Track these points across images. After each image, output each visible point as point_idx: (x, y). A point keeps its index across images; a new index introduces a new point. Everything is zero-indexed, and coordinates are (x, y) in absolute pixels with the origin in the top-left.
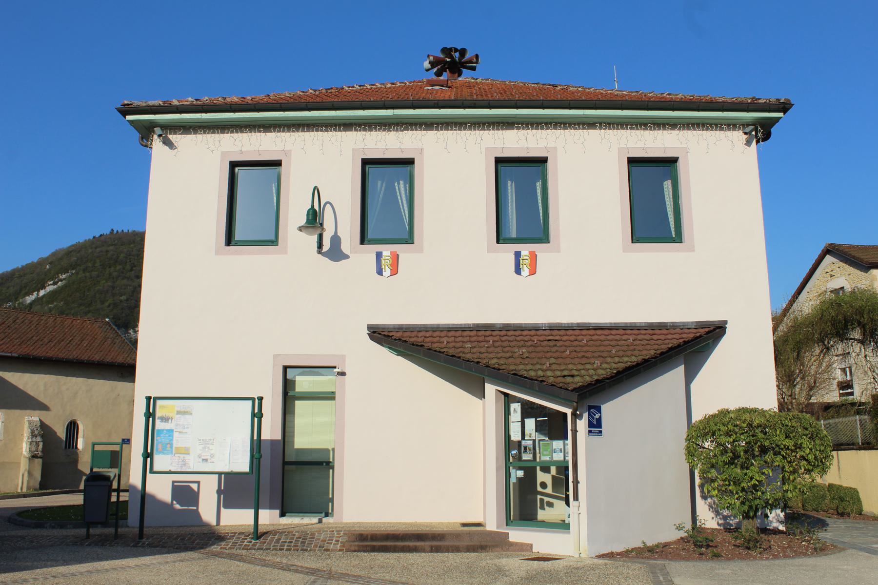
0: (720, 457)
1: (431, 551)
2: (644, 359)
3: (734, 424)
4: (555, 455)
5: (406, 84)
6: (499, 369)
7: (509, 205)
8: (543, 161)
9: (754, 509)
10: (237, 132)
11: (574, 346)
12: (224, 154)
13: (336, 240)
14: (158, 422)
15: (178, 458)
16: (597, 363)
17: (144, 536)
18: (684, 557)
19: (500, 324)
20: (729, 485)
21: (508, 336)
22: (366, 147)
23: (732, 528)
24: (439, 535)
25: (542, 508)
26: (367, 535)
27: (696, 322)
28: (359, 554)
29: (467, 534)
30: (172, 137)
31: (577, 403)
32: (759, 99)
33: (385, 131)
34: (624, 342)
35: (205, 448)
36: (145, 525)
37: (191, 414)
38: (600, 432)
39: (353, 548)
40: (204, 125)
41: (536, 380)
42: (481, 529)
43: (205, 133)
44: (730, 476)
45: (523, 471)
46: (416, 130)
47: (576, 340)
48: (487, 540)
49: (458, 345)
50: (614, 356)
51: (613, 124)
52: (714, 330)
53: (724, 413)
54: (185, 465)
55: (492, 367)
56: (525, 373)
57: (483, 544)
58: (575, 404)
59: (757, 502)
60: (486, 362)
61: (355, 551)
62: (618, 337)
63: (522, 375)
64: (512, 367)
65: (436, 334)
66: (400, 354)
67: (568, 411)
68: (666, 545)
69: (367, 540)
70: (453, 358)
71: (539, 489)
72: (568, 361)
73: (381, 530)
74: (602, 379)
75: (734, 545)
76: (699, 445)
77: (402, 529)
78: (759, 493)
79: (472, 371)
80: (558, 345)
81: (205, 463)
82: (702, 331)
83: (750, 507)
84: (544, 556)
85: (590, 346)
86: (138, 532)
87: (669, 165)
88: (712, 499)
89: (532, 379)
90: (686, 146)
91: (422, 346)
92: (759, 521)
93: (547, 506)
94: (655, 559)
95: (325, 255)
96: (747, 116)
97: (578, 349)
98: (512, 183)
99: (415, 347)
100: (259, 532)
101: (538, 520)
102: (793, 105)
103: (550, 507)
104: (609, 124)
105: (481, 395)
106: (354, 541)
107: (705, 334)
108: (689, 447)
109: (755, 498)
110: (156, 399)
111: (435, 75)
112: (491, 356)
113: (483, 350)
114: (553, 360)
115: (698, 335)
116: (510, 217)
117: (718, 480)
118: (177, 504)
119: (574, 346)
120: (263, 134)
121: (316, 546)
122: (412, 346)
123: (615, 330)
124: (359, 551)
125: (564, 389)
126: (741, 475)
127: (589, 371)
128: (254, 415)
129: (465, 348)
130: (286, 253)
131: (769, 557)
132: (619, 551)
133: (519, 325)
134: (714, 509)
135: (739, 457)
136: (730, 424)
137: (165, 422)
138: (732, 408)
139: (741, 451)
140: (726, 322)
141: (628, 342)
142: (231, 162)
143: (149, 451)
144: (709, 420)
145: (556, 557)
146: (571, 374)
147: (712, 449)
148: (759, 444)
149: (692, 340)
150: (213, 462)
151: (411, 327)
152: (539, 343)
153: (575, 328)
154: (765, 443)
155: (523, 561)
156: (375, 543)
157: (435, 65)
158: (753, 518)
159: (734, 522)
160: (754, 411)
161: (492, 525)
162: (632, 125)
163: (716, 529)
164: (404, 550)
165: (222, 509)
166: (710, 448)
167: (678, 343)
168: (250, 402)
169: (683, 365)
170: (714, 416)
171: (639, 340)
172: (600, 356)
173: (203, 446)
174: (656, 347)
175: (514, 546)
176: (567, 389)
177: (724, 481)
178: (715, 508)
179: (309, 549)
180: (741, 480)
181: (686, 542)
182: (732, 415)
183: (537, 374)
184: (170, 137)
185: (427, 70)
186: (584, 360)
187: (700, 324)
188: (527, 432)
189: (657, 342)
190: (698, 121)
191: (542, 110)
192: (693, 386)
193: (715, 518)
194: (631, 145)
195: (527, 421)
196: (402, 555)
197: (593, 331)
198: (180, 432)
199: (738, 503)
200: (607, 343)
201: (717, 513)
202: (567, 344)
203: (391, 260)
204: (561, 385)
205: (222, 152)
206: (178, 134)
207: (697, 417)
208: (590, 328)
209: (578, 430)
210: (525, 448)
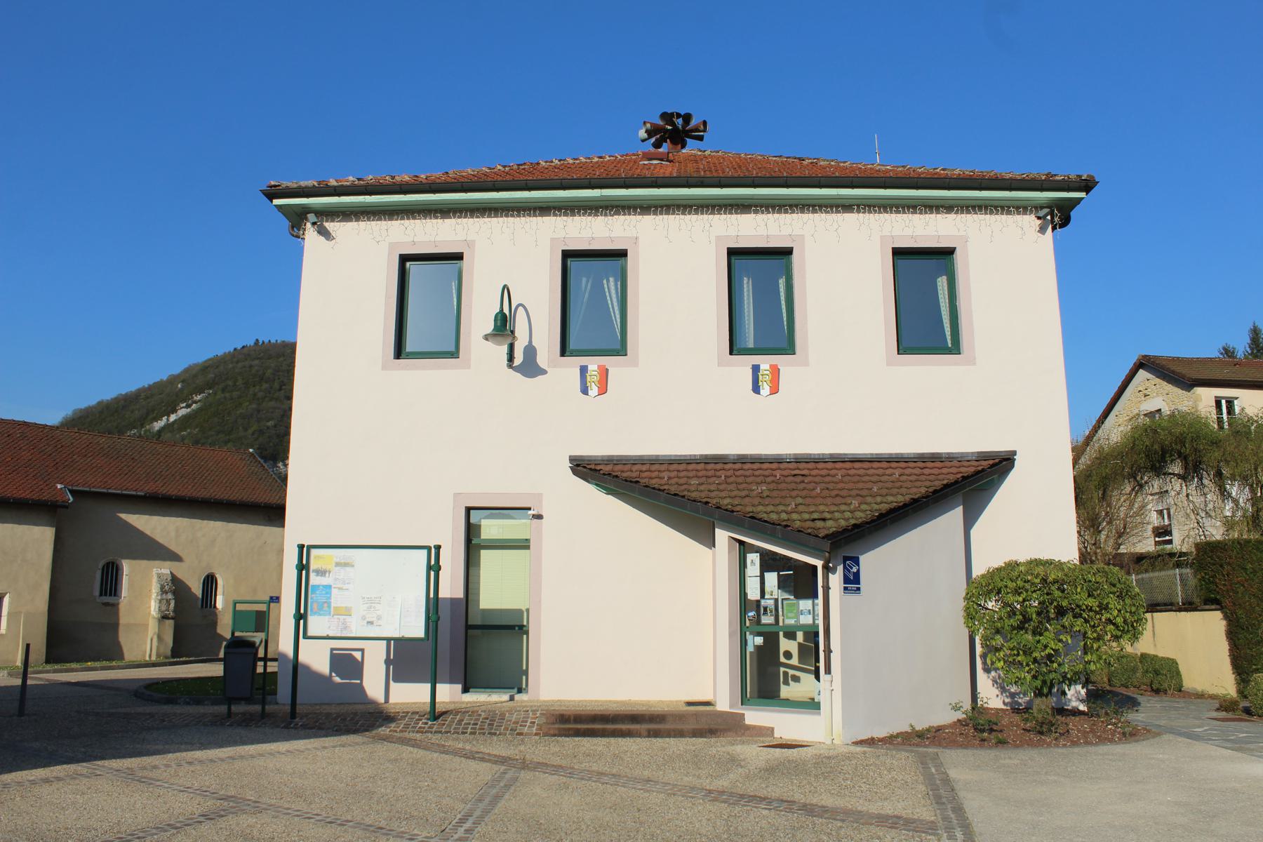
0: (1006, 620)
1: (649, 736)
6: (733, 511)
10: (408, 219)
11: (826, 483)
13: (530, 351)
14: (312, 575)
16: (855, 503)
17: (297, 715)
18: (961, 743)
19: (734, 455)
20: (1018, 655)
24: (658, 715)
25: (786, 683)
26: (569, 716)
29: (693, 715)
32: (1055, 175)
34: (888, 477)
36: (298, 702)
37: (353, 566)
38: (858, 589)
39: (552, 732)
41: (779, 525)
44: (1019, 644)
49: (682, 481)
51: (874, 207)
52: (1001, 462)
53: (1012, 565)
56: (765, 516)
58: (827, 554)
59: (1052, 676)
61: (555, 735)
64: (749, 509)
66: (610, 492)
67: (819, 563)
68: (939, 729)
71: (782, 659)
75: (1024, 729)
76: (980, 605)
77: (614, 709)
78: (1055, 665)
79: (698, 513)
81: (370, 626)
82: (985, 464)
83: (1044, 682)
84: (789, 743)
88: (996, 672)
89: (773, 524)
90: (964, 233)
92: (1054, 699)
93: (792, 680)
94: (926, 746)
95: (517, 369)
97: (831, 486)
98: (749, 280)
100: (437, 711)
104: (869, 206)
105: (711, 543)
107: (989, 468)
108: (968, 608)
109: (1050, 672)
110: (310, 547)
112: (723, 494)
113: (712, 487)
114: (799, 500)
115: (980, 468)
117: (1004, 648)
118: (337, 676)
119: (826, 483)
120: (440, 221)
121: (506, 729)
127: (845, 513)
128: (429, 568)
129: (690, 484)
130: (469, 368)
135: (1031, 620)
137: (321, 576)
140: (1014, 453)
141: (893, 478)
144: (993, 574)
145: (803, 744)
146: (823, 517)
147: (997, 610)
148: (1055, 604)
149: (972, 476)
150: (380, 626)
152: (782, 478)
153: (827, 460)
156: (579, 726)
158: (1047, 696)
160: (1049, 563)
163: (1002, 709)
165: (391, 682)
168: (425, 552)
170: (999, 570)
172: (858, 495)
174: (928, 483)
176: (817, 536)
177: (1012, 649)
178: (1001, 684)
179: (498, 732)
180: (1032, 649)
181: (964, 726)
182: (1022, 568)
184: (327, 225)
185: (643, 141)
186: (838, 500)
188: (767, 589)
190: (974, 203)
192: (973, 532)
193: (1000, 696)
195: (767, 575)
196: (612, 740)
197: (849, 463)
198: (339, 588)
199: (1029, 677)
200: (867, 478)
201: (1003, 689)
202: (817, 479)
204: (809, 531)
205: (390, 243)
207: (978, 570)
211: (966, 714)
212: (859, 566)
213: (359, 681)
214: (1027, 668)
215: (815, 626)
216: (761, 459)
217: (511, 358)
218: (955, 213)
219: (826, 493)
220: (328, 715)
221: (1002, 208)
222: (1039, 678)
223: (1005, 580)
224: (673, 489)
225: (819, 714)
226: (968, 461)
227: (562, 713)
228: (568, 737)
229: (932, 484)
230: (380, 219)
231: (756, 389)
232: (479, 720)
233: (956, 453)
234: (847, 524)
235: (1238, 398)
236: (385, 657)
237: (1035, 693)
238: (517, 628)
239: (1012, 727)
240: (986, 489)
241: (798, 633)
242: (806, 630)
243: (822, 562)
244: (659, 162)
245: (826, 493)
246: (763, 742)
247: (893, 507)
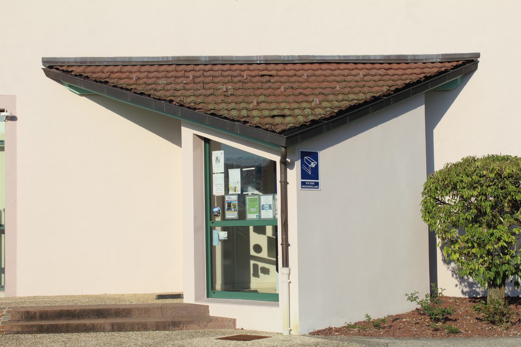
0: (461, 214)
1: (113, 330)
2: (374, 97)
3: (479, 174)
4: (263, 212)
6: (195, 109)
9: (502, 276)
11: (291, 82)
16: (317, 100)
18: (415, 333)
19: (205, 57)
20: (473, 247)
21: (214, 71)
23: (478, 296)
24: (124, 310)
25: (256, 275)
26: (35, 313)
27: (443, 55)
28: (22, 336)
29: (158, 308)
31: (285, 148)
34: (352, 77)
38: (317, 184)
39: (15, 329)
41: (238, 121)
42: (178, 302)
44: (473, 237)
45: (227, 232)
47: (295, 75)
48: (182, 315)
49: (150, 81)
50: (338, 93)
52: (464, 64)
53: (469, 161)
56: (225, 113)
57: (176, 320)
58: (283, 149)
59: (505, 267)
60: (180, 101)
61: (18, 333)
62: (346, 72)
63: (222, 115)
64: (211, 106)
65: (125, 69)
66: (83, 93)
67: (277, 159)
68: (397, 318)
69: (36, 318)
70: (143, 96)
71: (253, 253)
72: (281, 99)
74: (320, 119)
75: (477, 319)
76: (438, 200)
77: (84, 304)
78: (508, 257)
79: (163, 111)
82: (448, 65)
83: (497, 273)
84: (248, 334)
85: (311, 82)
89: (233, 120)
91: (106, 82)
92: (510, 288)
93: (262, 272)
94: (379, 337)
97: (295, 85)
99: (98, 84)
101: (251, 289)
105: (177, 140)
106: (19, 320)
107: (452, 69)
108: (426, 202)
109: (503, 263)
112: (189, 93)
113: (179, 87)
114: (262, 98)
115: (443, 69)
117: (459, 240)
119: (291, 82)
122: (94, 83)
123: (344, 64)
125: (271, 131)
126: (487, 235)
127: (305, 110)
129: (158, 84)
131: (516, 334)
132: (339, 327)
133: (228, 59)
134: (458, 275)
135: (485, 214)
136: (475, 174)
138: (480, 155)
139: (486, 206)
140: (478, 55)
141: (357, 78)
144: (449, 170)
145: (262, 335)
146: (282, 113)
147: (453, 204)
148: (509, 198)
149: (435, 76)
151: (97, 60)
152: (249, 78)
153: (296, 62)
154: (517, 196)
155: (219, 340)
156: (43, 323)
158: (500, 286)
160: (506, 159)
161: (189, 299)
163: (460, 299)
164: (78, 329)
166: (450, 203)
167: (418, 79)
169: (424, 106)
170: (456, 165)
171: (372, 75)
172: (320, 93)
174: (390, 83)
175: (214, 321)
176: (274, 132)
177: (467, 242)
180: (486, 242)
181: (421, 314)
182: (478, 164)
183: (240, 113)
186: (301, 98)
188: (231, 185)
189: (393, 78)
192: (437, 131)
193: (458, 286)
195: (231, 172)
196: (75, 336)
197: (317, 65)
199: (482, 269)
200: (331, 78)
201: (462, 280)
202: (283, 79)
204: (267, 126)
207: (439, 166)
209: (288, 181)
210: (229, 205)
211: (422, 305)
212: (317, 161)
214: (481, 260)
215: (275, 220)
219: (290, 91)
222: (492, 269)
223: (461, 175)
224: (140, 89)
225: (278, 305)
226: (432, 63)
229: (394, 83)
233: (421, 55)
234: (305, 120)
237: (489, 283)
239: (467, 316)
240: (450, 90)
242: (256, 225)
243: (280, 158)
245: (290, 91)
246: (224, 334)
247: (353, 104)
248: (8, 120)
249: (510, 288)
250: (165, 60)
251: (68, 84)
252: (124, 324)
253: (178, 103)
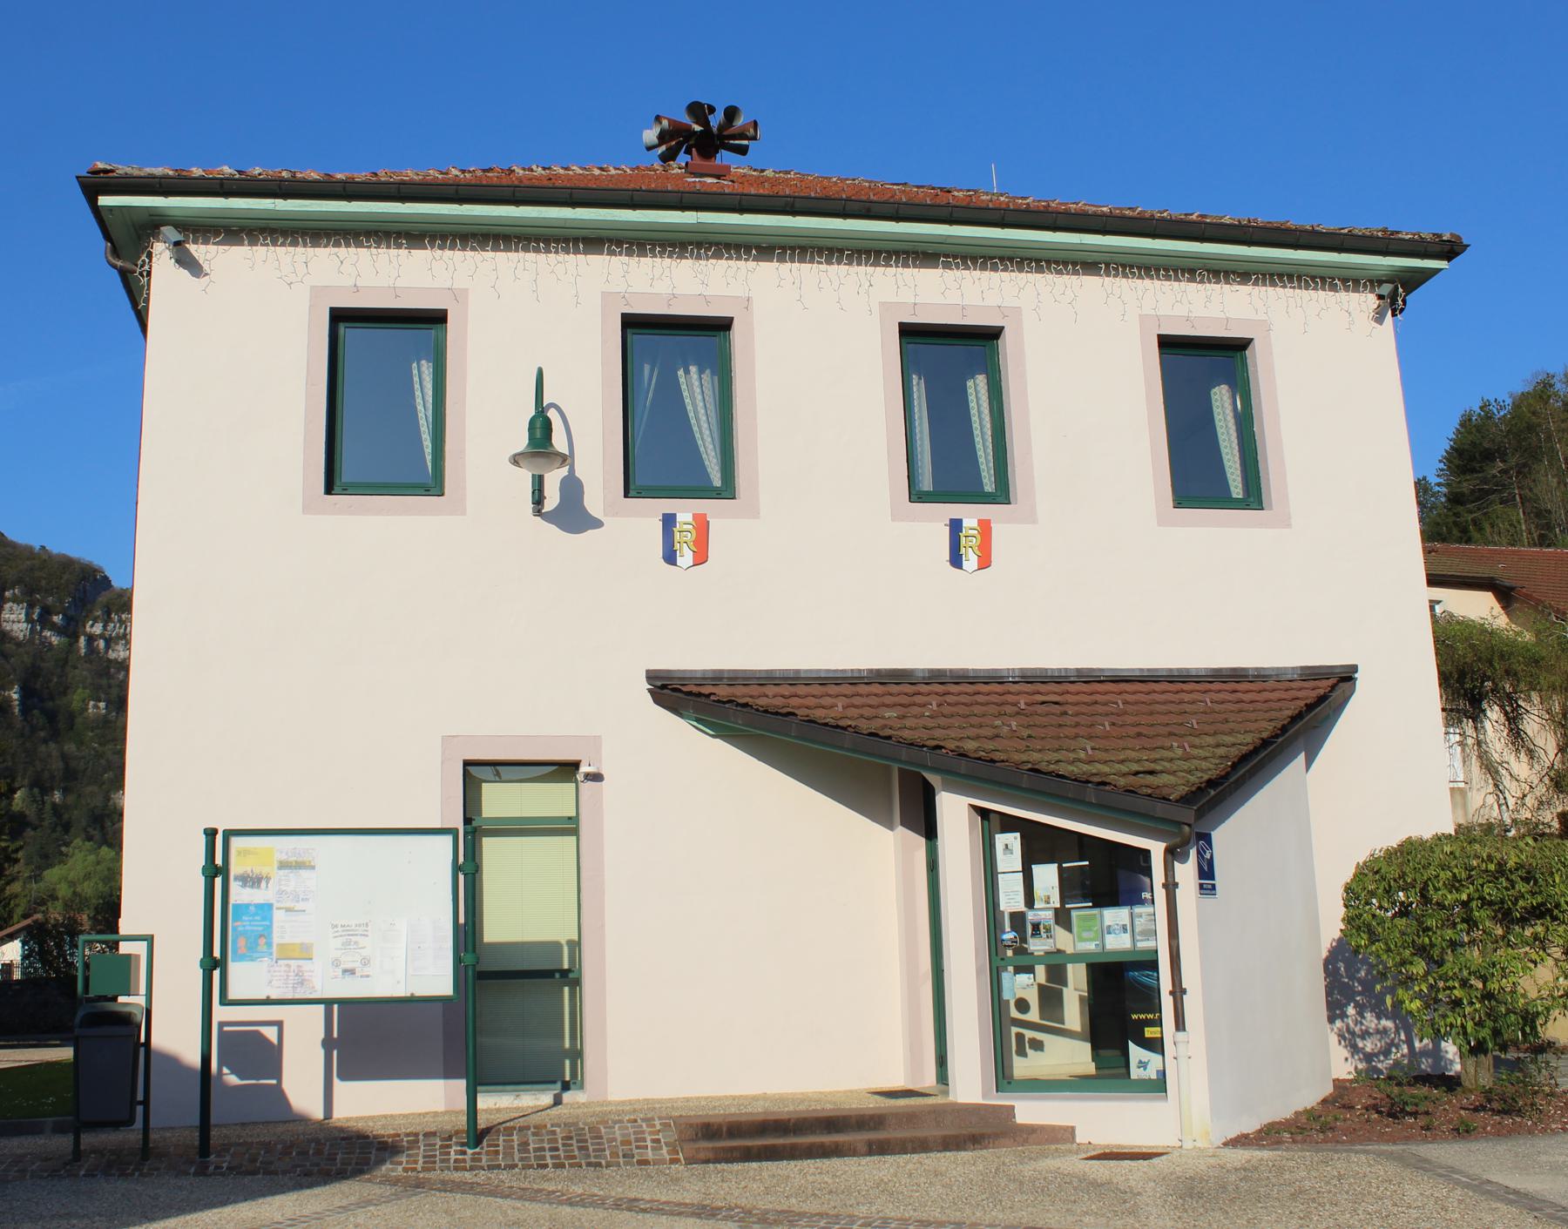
1: (870, 1153)
5: (625, 172)
7: (917, 424)
8: (992, 335)
10: (348, 245)
12: (316, 292)
13: (572, 488)
14: (234, 886)
15: (287, 969)
17: (211, 1150)
19: (923, 670)
22: (630, 290)
24: (872, 1117)
25: (1022, 1052)
26: (720, 1126)
29: (929, 1112)
30: (197, 250)
32: (1398, 232)
33: (672, 257)
35: (349, 943)
36: (213, 1120)
37: (313, 868)
38: (1214, 887)
39: (702, 1155)
40: (271, 226)
43: (274, 244)
46: (739, 258)
51: (1131, 267)
54: (302, 983)
55: (972, 755)
61: (707, 1161)
73: (800, 1111)
80: (1070, 712)
81: (348, 978)
86: (197, 1143)
87: (1230, 353)
88: (1343, 1021)
90: (1264, 317)
93: (1030, 1048)
95: (550, 517)
96: (1384, 263)
98: (920, 379)
100: (478, 1127)
102: (1468, 246)
103: (1036, 1050)
104: (1124, 266)
110: (229, 834)
111: (660, 158)
116: (919, 449)
118: (232, 1073)
120: (403, 252)
121: (614, 1154)
124: (717, 1161)
128: (456, 868)
130: (464, 513)
134: (1347, 1042)
137: (252, 887)
140: (1354, 668)
142: (332, 310)
143: (217, 953)
150: (368, 976)
153: (1072, 679)
157: (667, 137)
159: (1384, 1065)
162: (1166, 270)
165: (336, 1080)
168: (448, 839)
173: (340, 940)
178: (1350, 1040)
179: (603, 1162)
184: (192, 248)
185: (649, 148)
187: (1308, 672)
190: (1280, 269)
191: (999, 230)
193: (1349, 1060)
194: (1164, 311)
195: (1038, 870)
198: (288, 910)
201: (1354, 1049)
203: (694, 532)
205: (312, 288)
206: (214, 244)
208: (1102, 678)
210: (1036, 927)
213: (274, 1082)
216: (968, 677)
217: (538, 500)
218: (1253, 285)
220: (268, 1147)
221: (1323, 279)
227: (706, 1120)
228: (732, 1162)
230: (295, 244)
231: (956, 560)
232: (556, 1141)
235: (1440, 602)
236: (322, 1035)
238: (557, 975)
241: (1036, 966)
244: (715, 181)
248: (588, 780)
249: (1429, 1061)
250: (856, 675)
251: (696, 717)
252: (888, 1142)
253: (952, 751)
